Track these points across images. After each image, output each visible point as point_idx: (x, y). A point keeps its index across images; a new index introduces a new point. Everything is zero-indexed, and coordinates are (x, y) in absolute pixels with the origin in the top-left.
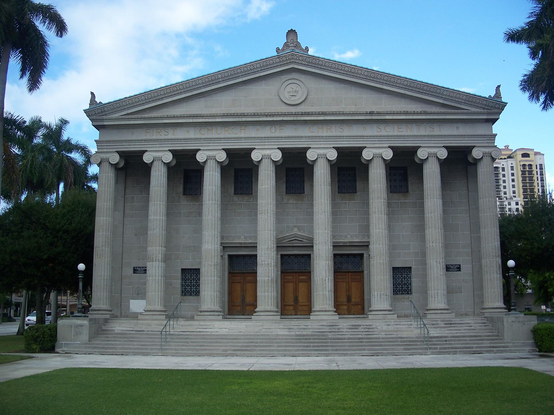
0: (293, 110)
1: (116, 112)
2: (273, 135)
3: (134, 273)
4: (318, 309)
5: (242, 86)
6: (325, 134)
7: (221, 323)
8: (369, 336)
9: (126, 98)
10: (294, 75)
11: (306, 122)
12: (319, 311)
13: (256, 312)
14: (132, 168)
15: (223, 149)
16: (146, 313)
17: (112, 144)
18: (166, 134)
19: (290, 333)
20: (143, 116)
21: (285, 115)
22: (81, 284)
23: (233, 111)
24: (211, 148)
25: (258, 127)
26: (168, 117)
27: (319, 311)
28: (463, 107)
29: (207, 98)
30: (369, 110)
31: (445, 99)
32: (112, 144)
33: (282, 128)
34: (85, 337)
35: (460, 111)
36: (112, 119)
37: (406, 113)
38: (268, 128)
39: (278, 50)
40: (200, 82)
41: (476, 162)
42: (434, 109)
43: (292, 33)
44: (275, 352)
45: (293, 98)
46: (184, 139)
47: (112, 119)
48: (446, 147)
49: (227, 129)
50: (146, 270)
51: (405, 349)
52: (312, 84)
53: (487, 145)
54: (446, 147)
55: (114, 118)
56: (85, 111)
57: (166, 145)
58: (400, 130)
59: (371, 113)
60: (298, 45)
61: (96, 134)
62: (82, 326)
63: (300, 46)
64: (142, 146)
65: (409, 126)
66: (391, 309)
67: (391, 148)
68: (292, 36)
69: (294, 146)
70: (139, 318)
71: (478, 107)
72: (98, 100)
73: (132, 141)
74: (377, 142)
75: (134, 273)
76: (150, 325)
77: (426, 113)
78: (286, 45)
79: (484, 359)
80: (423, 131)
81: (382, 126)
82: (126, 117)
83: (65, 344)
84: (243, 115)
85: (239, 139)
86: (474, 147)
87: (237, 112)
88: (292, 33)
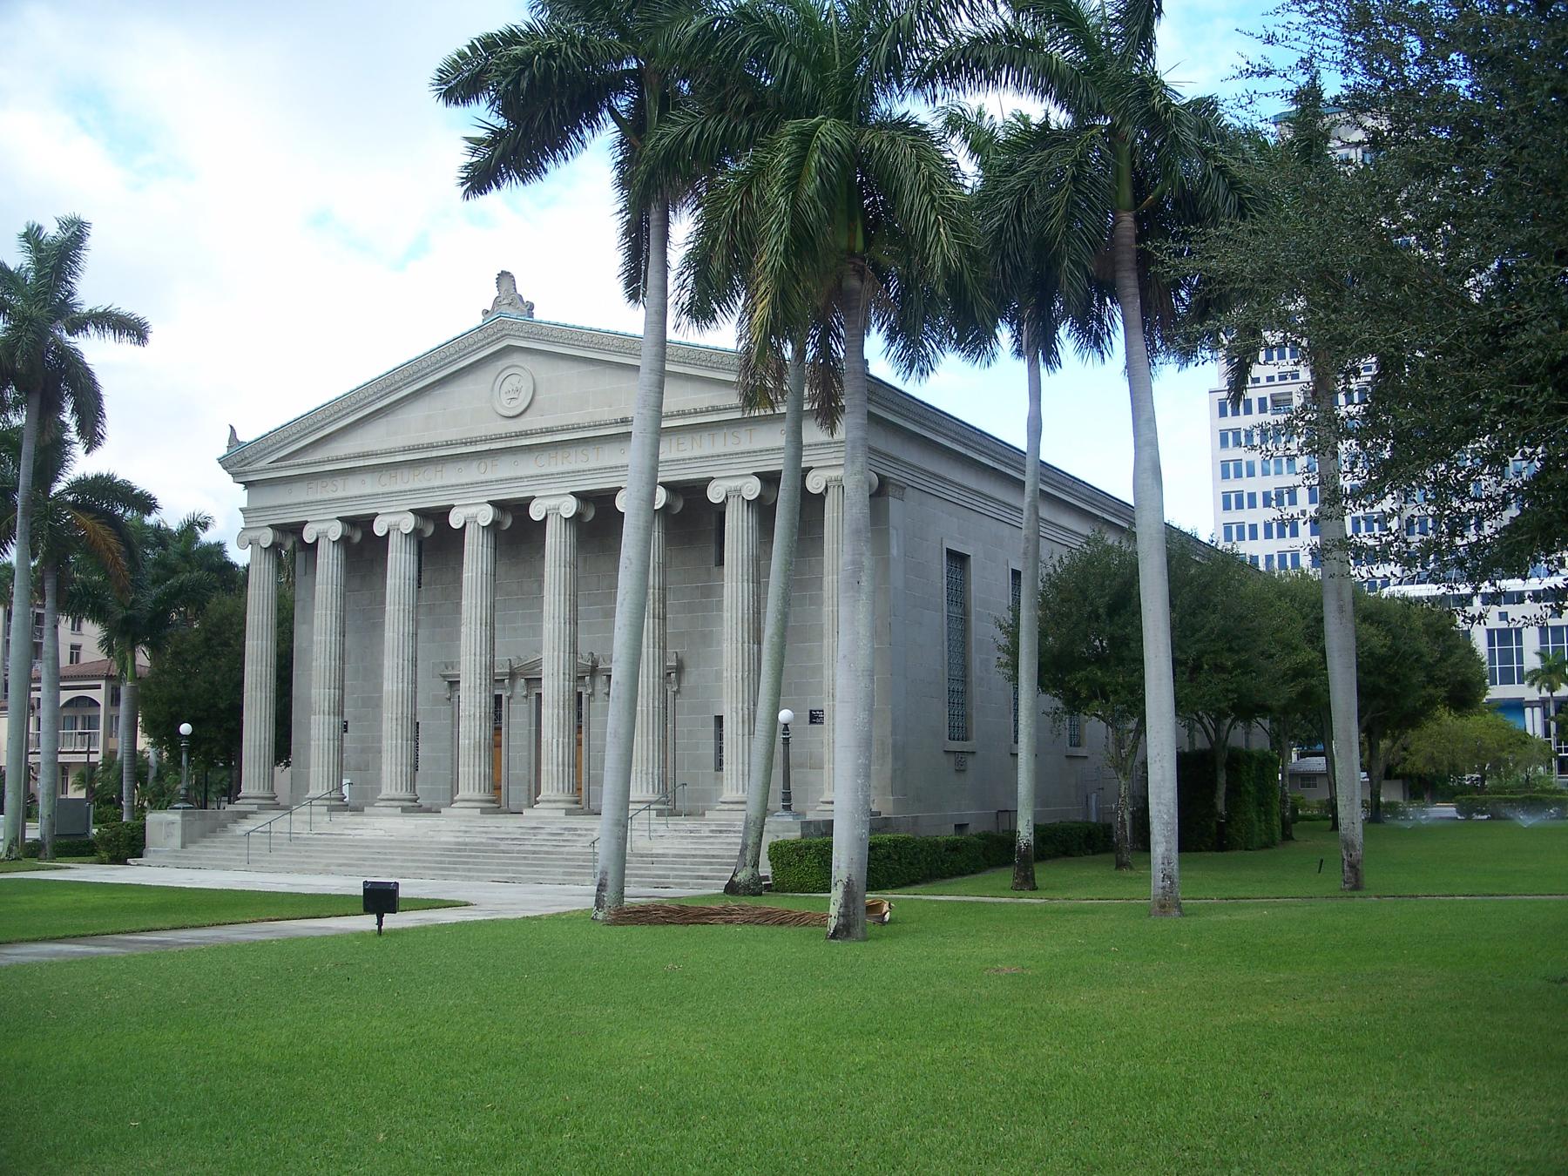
6: (593, 464)
7: (400, 820)
14: (290, 549)
16: (607, 800)
20: (300, 461)
21: (508, 437)
22: (184, 757)
23: (426, 439)
29: (391, 418)
30: (619, 416)
34: (176, 841)
37: (716, 410)
45: (514, 403)
46: (357, 495)
51: (565, 874)
52: (544, 371)
55: (262, 468)
56: (220, 461)
58: (682, 447)
61: (240, 496)
65: (697, 436)
68: (505, 283)
72: (240, 437)
73: (290, 504)
78: (496, 302)
85: (430, 488)
88: (504, 277)
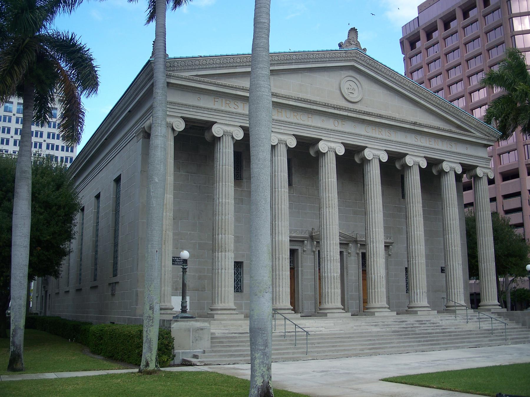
0: (351, 106)
1: (185, 70)
2: (336, 128)
3: (442, 272)
4: (379, 306)
5: (307, 72)
8: (444, 331)
9: (201, 57)
10: (351, 73)
11: (363, 121)
12: (379, 308)
13: (479, 306)
15: (294, 135)
17: (176, 107)
18: (236, 107)
19: (382, 330)
20: (213, 81)
24: (282, 131)
25: (468, 146)
26: (359, 112)
27: (379, 308)
28: (472, 131)
31: (462, 122)
32: (176, 107)
33: (343, 123)
35: (468, 133)
36: (181, 78)
38: (332, 121)
39: (365, 50)
40: (276, 58)
41: (216, 140)
42: (447, 127)
43: (353, 31)
44: (410, 348)
45: (351, 95)
47: (181, 78)
48: (184, 118)
49: (295, 114)
50: (173, 261)
53: (485, 166)
54: (184, 118)
57: (237, 120)
59: (415, 124)
60: (358, 44)
62: (202, 329)
63: (360, 46)
64: (211, 116)
66: (235, 308)
67: (184, 119)
68: (353, 34)
69: (354, 143)
70: (215, 318)
71: (482, 133)
74: (416, 151)
75: (442, 272)
76: (241, 326)
77: (438, 129)
78: (348, 41)
79: (210, 368)
80: (411, 139)
81: (419, 137)
82: (198, 78)
83: (183, 353)
84: (381, 116)
86: (366, 147)
87: (311, 99)
88: (353, 31)
